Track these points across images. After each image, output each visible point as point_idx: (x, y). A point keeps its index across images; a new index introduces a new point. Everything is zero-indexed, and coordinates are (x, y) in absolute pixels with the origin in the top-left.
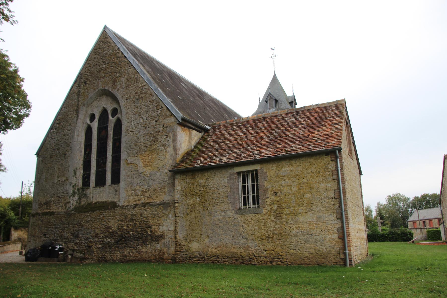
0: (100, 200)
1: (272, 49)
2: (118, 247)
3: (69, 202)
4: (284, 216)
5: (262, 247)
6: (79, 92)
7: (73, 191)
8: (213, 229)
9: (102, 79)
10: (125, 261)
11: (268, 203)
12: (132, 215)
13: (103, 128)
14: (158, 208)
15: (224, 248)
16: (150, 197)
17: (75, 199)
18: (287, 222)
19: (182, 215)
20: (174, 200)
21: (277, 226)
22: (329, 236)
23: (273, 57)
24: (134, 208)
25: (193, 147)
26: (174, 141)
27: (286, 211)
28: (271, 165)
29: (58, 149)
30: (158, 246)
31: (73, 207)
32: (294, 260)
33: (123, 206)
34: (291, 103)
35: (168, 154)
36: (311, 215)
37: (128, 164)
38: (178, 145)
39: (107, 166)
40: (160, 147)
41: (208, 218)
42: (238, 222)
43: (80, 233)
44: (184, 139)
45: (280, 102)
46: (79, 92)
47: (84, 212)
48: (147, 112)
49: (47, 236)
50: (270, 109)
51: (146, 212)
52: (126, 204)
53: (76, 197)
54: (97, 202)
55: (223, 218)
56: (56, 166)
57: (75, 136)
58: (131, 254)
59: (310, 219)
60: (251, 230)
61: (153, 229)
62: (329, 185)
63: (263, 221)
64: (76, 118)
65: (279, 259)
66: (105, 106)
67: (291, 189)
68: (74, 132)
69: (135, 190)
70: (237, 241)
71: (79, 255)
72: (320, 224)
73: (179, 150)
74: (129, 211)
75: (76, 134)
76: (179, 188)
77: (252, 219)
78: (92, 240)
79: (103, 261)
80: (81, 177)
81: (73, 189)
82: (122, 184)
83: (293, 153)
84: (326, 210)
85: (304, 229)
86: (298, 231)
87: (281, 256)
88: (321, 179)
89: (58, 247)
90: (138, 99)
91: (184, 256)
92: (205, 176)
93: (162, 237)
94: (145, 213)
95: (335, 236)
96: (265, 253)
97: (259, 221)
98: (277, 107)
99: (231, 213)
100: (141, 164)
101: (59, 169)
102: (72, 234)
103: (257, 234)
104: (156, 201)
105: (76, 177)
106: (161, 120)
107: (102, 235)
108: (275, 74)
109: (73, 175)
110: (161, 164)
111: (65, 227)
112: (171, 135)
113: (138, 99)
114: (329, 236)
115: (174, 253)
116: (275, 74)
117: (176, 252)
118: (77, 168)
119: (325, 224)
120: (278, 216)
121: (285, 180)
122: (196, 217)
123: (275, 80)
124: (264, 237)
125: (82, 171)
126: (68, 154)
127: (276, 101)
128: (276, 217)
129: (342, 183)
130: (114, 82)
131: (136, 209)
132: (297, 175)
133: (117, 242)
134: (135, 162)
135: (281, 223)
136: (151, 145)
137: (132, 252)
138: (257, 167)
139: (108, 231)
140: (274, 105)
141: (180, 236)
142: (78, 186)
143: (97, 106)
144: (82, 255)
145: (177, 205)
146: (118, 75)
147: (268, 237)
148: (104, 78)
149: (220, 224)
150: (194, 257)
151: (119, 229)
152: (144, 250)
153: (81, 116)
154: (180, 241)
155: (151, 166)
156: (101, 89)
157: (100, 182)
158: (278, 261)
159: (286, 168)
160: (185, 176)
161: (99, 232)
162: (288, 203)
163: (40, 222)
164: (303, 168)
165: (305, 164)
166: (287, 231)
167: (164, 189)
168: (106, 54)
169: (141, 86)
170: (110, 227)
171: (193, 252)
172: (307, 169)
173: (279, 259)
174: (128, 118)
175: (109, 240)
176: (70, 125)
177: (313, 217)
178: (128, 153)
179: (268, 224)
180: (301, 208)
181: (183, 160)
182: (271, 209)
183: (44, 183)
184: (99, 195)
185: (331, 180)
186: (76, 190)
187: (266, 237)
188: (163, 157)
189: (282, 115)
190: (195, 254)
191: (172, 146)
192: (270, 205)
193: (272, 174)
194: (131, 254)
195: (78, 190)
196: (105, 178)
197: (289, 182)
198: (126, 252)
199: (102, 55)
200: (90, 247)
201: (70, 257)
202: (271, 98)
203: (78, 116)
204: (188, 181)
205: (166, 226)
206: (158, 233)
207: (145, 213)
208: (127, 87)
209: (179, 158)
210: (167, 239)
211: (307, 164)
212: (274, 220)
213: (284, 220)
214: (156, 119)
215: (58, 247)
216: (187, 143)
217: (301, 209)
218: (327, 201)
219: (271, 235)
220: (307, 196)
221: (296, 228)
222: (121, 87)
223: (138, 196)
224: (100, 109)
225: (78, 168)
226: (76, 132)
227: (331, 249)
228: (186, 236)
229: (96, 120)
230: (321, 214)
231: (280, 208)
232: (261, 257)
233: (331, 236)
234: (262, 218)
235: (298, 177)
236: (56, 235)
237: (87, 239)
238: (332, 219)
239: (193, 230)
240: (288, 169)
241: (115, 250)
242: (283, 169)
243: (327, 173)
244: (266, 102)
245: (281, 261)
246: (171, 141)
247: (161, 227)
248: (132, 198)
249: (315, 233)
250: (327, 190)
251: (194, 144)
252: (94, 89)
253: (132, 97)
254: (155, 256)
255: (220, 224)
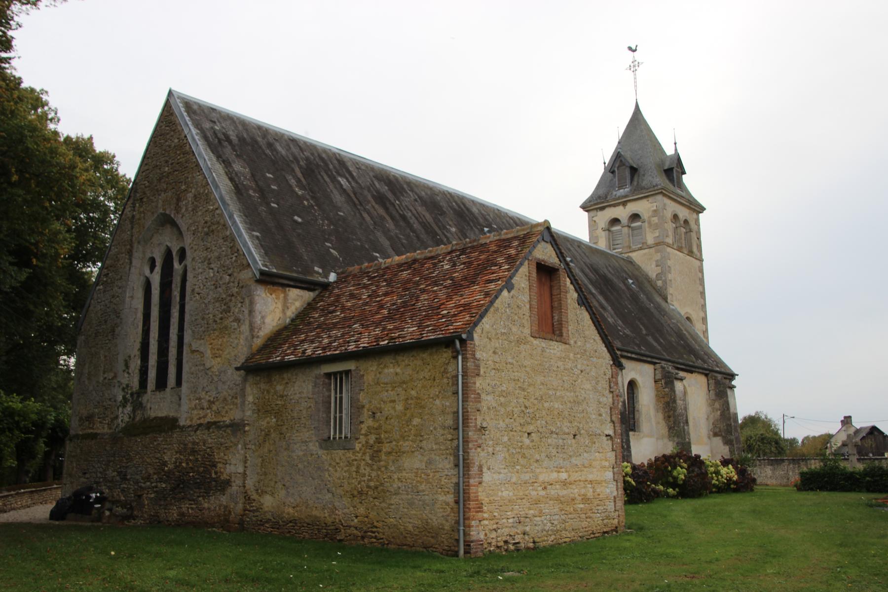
0: (160, 415)
1: (630, 49)
2: (174, 498)
3: (117, 417)
4: (384, 457)
5: (352, 509)
6: (133, 216)
7: (124, 397)
8: (290, 474)
9: (163, 194)
10: (183, 524)
11: (363, 432)
12: (194, 443)
13: (166, 285)
14: (225, 431)
15: (304, 508)
16: (218, 412)
17: (126, 412)
18: (386, 468)
19: (253, 447)
20: (244, 421)
21: (374, 474)
22: (442, 498)
23: (634, 67)
24: (195, 432)
25: (288, 321)
26: (251, 312)
27: (386, 448)
28: (370, 363)
29: (106, 322)
30: (224, 500)
31: (124, 425)
32: (393, 537)
33: (184, 426)
34: (669, 172)
35: (242, 336)
36: (420, 456)
37: (193, 352)
38: (258, 320)
39: (170, 354)
40: (233, 324)
41: (285, 453)
42: (323, 463)
43: (129, 471)
44: (272, 308)
45: (641, 171)
46: (133, 216)
47: (135, 436)
48: (219, 258)
49: (87, 476)
50: (620, 188)
51: (211, 438)
52: (188, 423)
53: (129, 408)
54: (155, 418)
55: (304, 455)
56: (102, 352)
57: (127, 299)
58: (190, 511)
59: (417, 465)
60: (339, 478)
61: (218, 469)
62: (448, 404)
63: (355, 463)
64: (128, 267)
65: (374, 532)
66: (169, 245)
67: (394, 408)
68: (125, 292)
69: (200, 399)
70: (320, 496)
71: (119, 510)
72: (431, 474)
73: (260, 329)
74: (189, 435)
75: (128, 295)
76: (250, 399)
77: (341, 459)
78: (143, 485)
79: (156, 522)
80: (137, 371)
81: (123, 394)
82: (185, 385)
83: (398, 342)
84: (440, 449)
85: (409, 481)
86: (400, 484)
87: (376, 527)
88: (436, 390)
89: (94, 495)
90: (207, 234)
91: (254, 519)
92: (283, 379)
93: (228, 483)
94: (210, 441)
95: (450, 498)
96: (356, 520)
97: (350, 464)
98: (635, 183)
99: (314, 447)
100: (208, 353)
101: (105, 357)
102: (119, 473)
103: (346, 487)
104: (225, 419)
105: (128, 373)
106: (235, 274)
107: (155, 476)
108: (637, 106)
109: (124, 368)
110: (233, 354)
111: (109, 461)
112: (247, 301)
113: (207, 234)
114: (442, 498)
115: (242, 513)
116: (637, 106)
117: (245, 510)
118: (130, 357)
119: (438, 475)
120: (375, 456)
121: (387, 391)
122: (270, 451)
123: (637, 121)
124: (356, 493)
125: (139, 362)
126: (117, 330)
127: (634, 170)
128: (372, 458)
129: (463, 401)
130: (179, 200)
131: (198, 432)
132: (404, 382)
133: (173, 490)
134: (202, 349)
135: (379, 469)
136: (221, 319)
137: (192, 509)
138: (351, 366)
139: (163, 470)
140: (628, 181)
141: (250, 483)
142: (132, 388)
143: (159, 244)
144: (125, 510)
145: (247, 428)
146: (183, 187)
147: (361, 493)
148: (165, 191)
149: (300, 466)
150: (266, 522)
151: (176, 467)
152: (206, 505)
153: (136, 262)
154: (249, 493)
155: (220, 356)
156: (161, 214)
157: (161, 384)
158: (372, 537)
159: (393, 369)
160: (258, 378)
161: (151, 472)
162: (390, 432)
163: (78, 451)
164: (413, 370)
165: (415, 362)
166: (386, 484)
167: (236, 398)
168: (170, 146)
169: (213, 210)
170: (165, 464)
171: (266, 512)
172: (418, 372)
173: (374, 532)
174: (194, 269)
175: (164, 486)
176: (121, 278)
177: (421, 461)
178: (193, 332)
179: (362, 471)
180: (407, 443)
181: (265, 347)
182: (367, 442)
183: (87, 382)
184: (158, 406)
185: (450, 393)
186: (128, 396)
187: (359, 493)
188: (236, 341)
189: (439, 255)
190: (268, 517)
191: (247, 322)
192: (366, 435)
193: (370, 379)
194: (190, 511)
195: (132, 395)
196: (167, 374)
197: (392, 394)
198: (185, 507)
199: (164, 148)
200: (140, 496)
201: (107, 513)
202: (622, 164)
203: (131, 263)
204: (263, 386)
205: (233, 465)
206: (224, 477)
207: (210, 441)
208: (195, 210)
209: (258, 342)
210: (234, 488)
211: (419, 362)
212: (370, 462)
213: (382, 463)
214: (230, 272)
215: (94, 495)
216: (278, 314)
217: (406, 445)
218: (442, 432)
219: (365, 489)
220: (416, 421)
221: (399, 479)
222: (187, 210)
223: (203, 409)
224: (163, 249)
225: (132, 356)
226: (128, 290)
227: (444, 522)
228: (257, 484)
229: (158, 269)
230: (433, 456)
231: (379, 441)
232: (350, 527)
233: (444, 498)
234: (353, 458)
235: (404, 386)
236: (99, 475)
237: (137, 482)
238: (448, 466)
239: (265, 474)
240: (392, 370)
241: (171, 504)
242: (386, 371)
243: (445, 380)
244: (613, 172)
245: (375, 537)
246: (246, 312)
247: (227, 466)
248: (195, 412)
249: (424, 491)
250: (443, 412)
251: (293, 316)
252: (153, 213)
253: (200, 229)
254: (219, 516)
255: (300, 466)
